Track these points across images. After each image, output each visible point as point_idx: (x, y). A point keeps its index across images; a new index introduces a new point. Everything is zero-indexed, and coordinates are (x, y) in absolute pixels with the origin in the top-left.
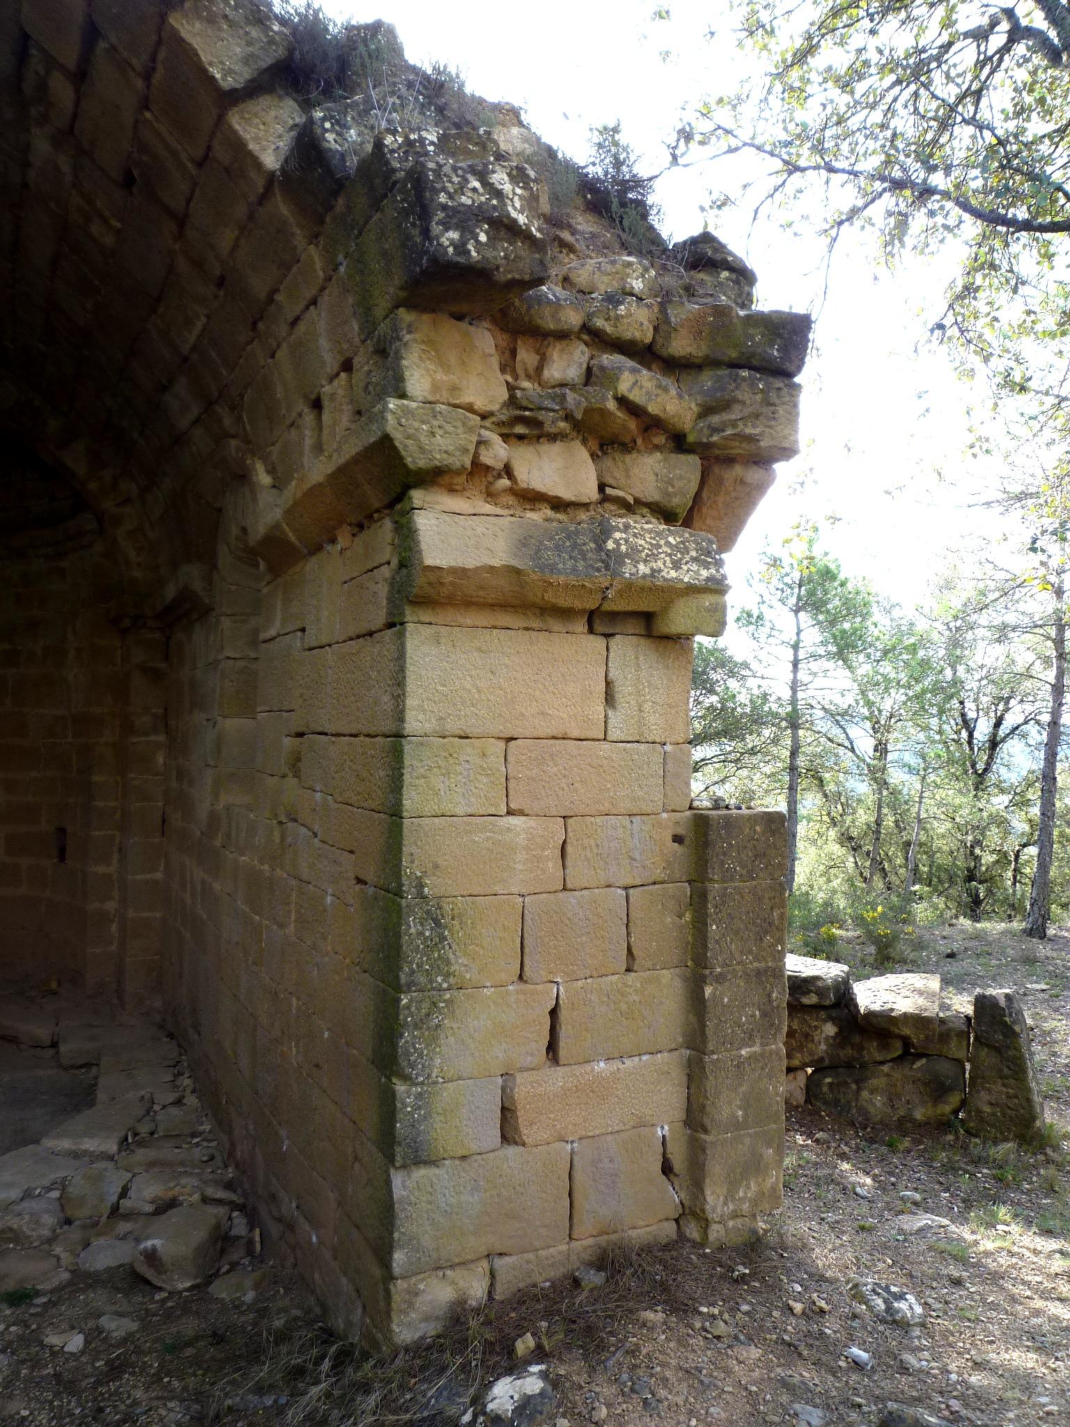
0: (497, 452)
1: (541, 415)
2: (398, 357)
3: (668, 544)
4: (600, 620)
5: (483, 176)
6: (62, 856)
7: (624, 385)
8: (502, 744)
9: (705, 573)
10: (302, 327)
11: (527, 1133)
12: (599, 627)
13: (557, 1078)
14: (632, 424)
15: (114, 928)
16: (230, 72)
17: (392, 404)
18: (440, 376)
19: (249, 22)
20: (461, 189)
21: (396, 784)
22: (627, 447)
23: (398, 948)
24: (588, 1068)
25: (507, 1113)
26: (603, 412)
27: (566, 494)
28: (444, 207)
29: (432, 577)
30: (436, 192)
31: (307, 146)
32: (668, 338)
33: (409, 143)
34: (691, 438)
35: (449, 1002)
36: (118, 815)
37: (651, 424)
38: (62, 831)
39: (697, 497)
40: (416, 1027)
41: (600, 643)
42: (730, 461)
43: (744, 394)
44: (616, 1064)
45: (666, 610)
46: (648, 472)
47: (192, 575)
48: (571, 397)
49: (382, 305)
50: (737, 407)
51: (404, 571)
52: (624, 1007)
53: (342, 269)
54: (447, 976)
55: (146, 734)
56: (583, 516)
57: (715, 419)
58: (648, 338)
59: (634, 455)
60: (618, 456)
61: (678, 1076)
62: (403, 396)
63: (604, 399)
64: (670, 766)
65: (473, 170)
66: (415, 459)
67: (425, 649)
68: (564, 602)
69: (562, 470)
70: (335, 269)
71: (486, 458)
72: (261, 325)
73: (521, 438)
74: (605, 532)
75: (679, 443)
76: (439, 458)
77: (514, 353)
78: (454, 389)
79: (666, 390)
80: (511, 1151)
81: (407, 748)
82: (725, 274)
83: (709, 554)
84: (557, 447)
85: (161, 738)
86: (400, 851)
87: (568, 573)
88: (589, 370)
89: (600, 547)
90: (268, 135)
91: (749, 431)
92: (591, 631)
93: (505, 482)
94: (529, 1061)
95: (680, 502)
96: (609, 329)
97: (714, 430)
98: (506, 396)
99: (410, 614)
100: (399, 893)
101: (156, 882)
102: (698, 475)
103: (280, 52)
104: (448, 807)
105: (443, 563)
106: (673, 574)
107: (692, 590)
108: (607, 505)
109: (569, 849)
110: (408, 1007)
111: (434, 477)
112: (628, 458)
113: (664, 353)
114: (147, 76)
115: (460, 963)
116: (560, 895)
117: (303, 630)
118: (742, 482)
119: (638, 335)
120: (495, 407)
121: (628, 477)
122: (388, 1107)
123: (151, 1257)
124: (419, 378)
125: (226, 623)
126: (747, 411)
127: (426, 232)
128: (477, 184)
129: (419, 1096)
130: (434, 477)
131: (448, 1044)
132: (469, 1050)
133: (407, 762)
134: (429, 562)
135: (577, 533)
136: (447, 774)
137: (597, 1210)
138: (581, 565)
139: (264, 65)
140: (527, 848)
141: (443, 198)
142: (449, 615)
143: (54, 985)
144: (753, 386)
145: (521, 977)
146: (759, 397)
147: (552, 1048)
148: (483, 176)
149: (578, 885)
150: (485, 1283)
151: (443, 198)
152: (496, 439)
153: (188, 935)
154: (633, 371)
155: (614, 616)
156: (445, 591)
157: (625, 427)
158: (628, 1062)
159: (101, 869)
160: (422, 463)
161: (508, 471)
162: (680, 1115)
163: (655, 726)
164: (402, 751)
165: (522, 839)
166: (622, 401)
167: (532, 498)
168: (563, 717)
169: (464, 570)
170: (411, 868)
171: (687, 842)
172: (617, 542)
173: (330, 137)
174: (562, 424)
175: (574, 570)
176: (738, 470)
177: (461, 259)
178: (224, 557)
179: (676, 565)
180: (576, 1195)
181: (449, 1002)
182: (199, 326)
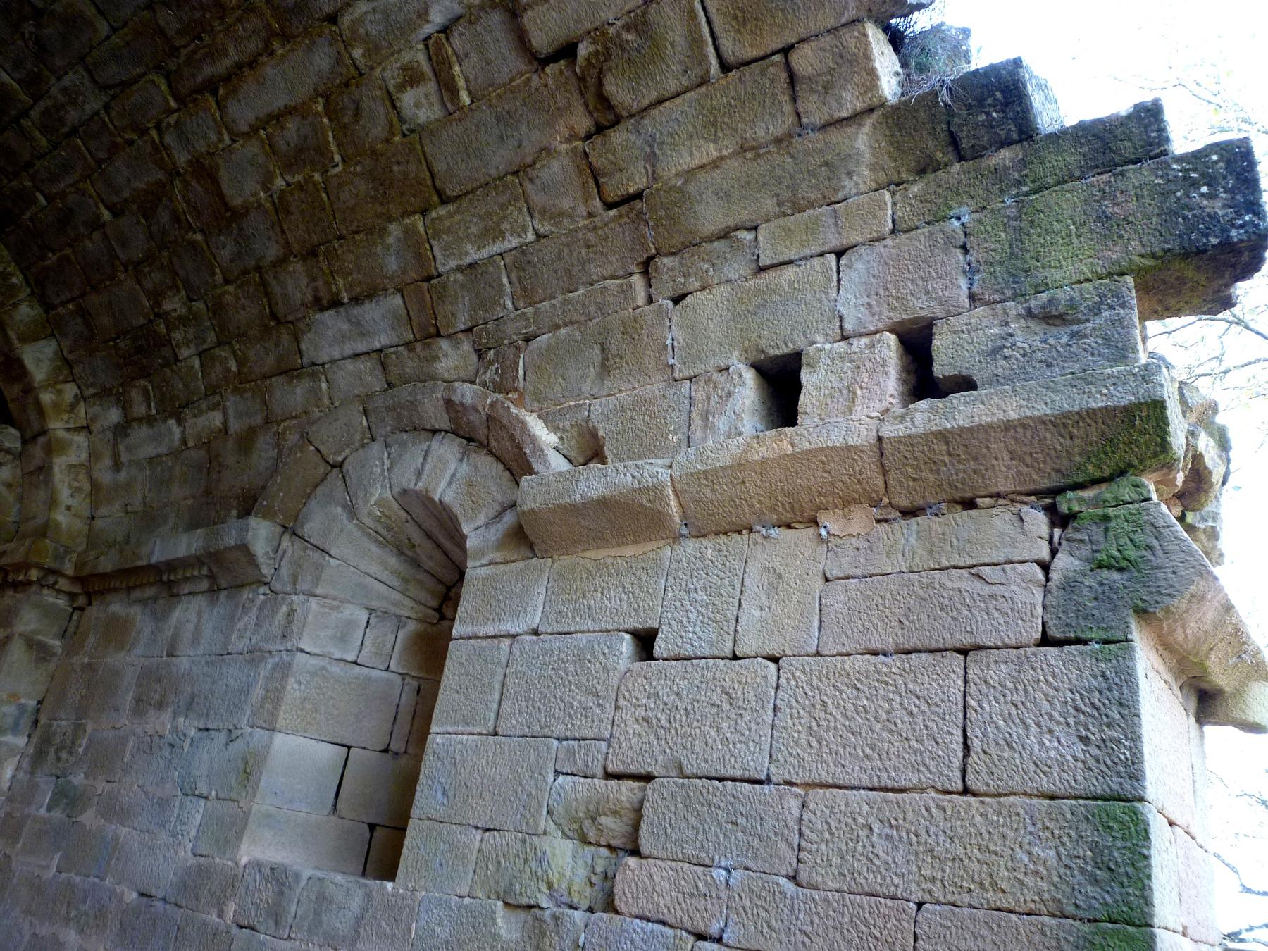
85: (21, 741)
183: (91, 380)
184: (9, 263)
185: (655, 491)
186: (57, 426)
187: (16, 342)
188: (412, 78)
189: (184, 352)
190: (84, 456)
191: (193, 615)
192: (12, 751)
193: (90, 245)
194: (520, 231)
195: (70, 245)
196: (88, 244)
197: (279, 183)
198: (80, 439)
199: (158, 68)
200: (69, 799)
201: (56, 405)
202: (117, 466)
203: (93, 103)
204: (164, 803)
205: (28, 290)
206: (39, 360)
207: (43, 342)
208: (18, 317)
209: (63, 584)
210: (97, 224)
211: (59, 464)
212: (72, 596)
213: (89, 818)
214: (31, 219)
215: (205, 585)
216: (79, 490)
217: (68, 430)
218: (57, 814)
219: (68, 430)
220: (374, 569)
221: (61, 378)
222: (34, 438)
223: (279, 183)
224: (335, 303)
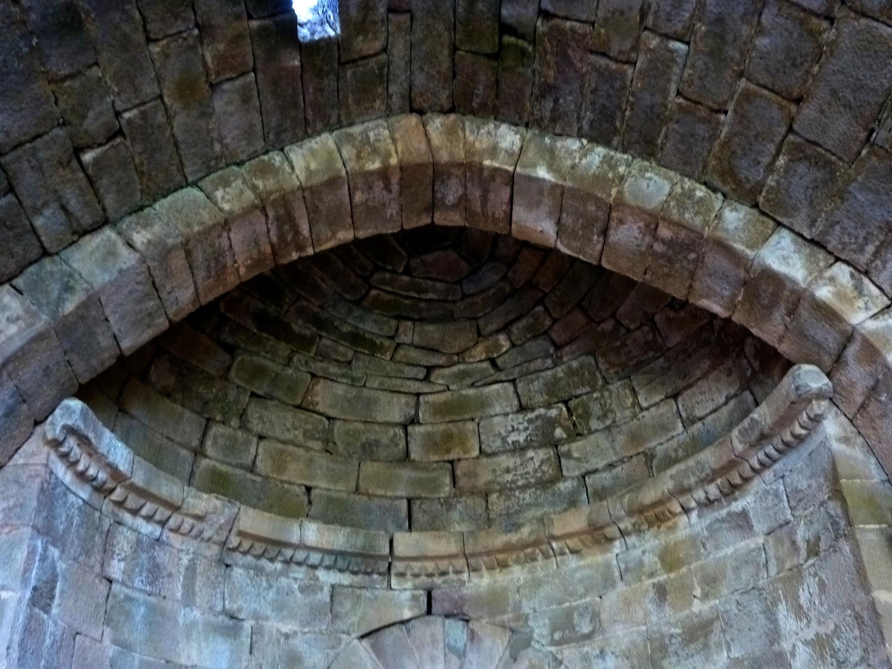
183: (862, 234)
184: (682, 181)
187: (749, 252)
195: (741, 75)
196: (763, 42)
201: (840, 295)
205: (720, 196)
206: (785, 258)
207: (774, 238)
208: (731, 227)
214: (679, 93)
217: (874, 316)
219: (874, 316)
221: (822, 264)
222: (839, 359)
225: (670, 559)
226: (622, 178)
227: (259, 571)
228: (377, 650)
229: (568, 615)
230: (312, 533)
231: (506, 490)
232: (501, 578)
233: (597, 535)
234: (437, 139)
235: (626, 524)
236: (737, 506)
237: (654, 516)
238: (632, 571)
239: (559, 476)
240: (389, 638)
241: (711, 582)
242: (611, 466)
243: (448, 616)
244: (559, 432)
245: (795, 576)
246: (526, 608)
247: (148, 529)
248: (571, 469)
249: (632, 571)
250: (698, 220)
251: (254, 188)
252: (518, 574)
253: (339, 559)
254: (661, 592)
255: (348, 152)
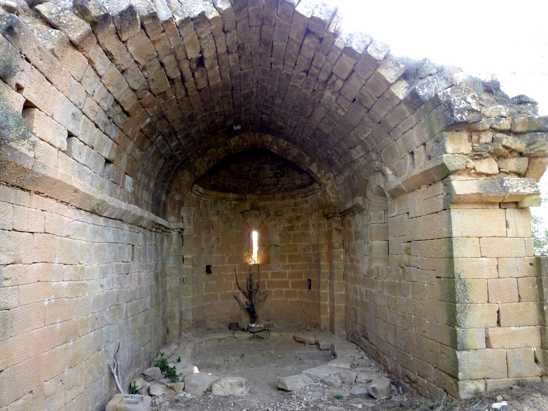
0: (472, 164)
1: (482, 153)
2: (444, 143)
3: (521, 183)
4: (503, 205)
5: (465, 100)
6: (310, 287)
7: (504, 142)
8: (478, 239)
9: (533, 190)
10: (407, 134)
11: (493, 345)
12: (502, 206)
13: (500, 330)
14: (507, 151)
15: (329, 310)
16: (392, 79)
17: (445, 155)
18: (455, 147)
19: (395, 66)
20: (460, 104)
21: (451, 249)
22: (505, 157)
23: (455, 292)
24: (509, 328)
25: (487, 339)
26: (499, 150)
27: (490, 172)
28: (457, 109)
29: (458, 197)
30: (454, 106)
31: (414, 95)
32: (515, 127)
33: (444, 93)
34: (524, 153)
35: (469, 307)
36: (328, 274)
37: (512, 151)
38: (310, 280)
39: (528, 169)
40: (461, 313)
41: (503, 211)
42: (537, 157)
43: (540, 139)
44: (517, 328)
45: (522, 201)
46: (512, 164)
47: (359, 200)
48: (490, 147)
49: (437, 131)
50: (538, 143)
51: (449, 196)
52: (519, 312)
53: (422, 121)
54: (468, 300)
55: (338, 249)
56: (495, 177)
57: (531, 147)
58: (509, 128)
59: (508, 159)
60: (503, 160)
61: (538, 333)
62: (446, 153)
63: (499, 146)
64: (527, 244)
65: (462, 99)
66: (451, 168)
67: (456, 215)
68: (493, 201)
69: (488, 166)
70: (421, 121)
71: (469, 166)
72: (391, 133)
73: (476, 159)
74: (502, 181)
75: (521, 154)
76: (457, 167)
77: (471, 137)
78: (458, 149)
79: (516, 142)
80: (489, 349)
81: (453, 240)
82: (529, 104)
83: (533, 184)
84: (486, 160)
85: (342, 250)
86: (453, 267)
87: (494, 194)
88: (493, 139)
89: (502, 186)
90: (401, 91)
91: (542, 149)
92: (500, 208)
93: (473, 171)
94: (492, 325)
95: (522, 171)
96: (498, 128)
97: (531, 150)
98: (472, 149)
99: (451, 207)
100: (454, 278)
101: (342, 294)
102: (528, 162)
103: (403, 72)
104: (465, 255)
105: (461, 193)
106: (523, 191)
107: (530, 195)
108: (501, 174)
109: (499, 267)
110: (458, 307)
111: (456, 172)
112: (506, 160)
113: (514, 131)
114: (366, 80)
115: (471, 296)
116: (498, 279)
117: (408, 213)
118: (541, 163)
119: (506, 128)
120: (469, 152)
121: (506, 165)
122: (454, 334)
123: (374, 389)
124: (450, 148)
125: (371, 213)
126: (541, 144)
127: (452, 116)
128: (464, 102)
129: (463, 331)
130: (456, 172)
131: (470, 318)
132: (475, 322)
133: (454, 244)
134: (457, 193)
135: (495, 182)
136: (464, 247)
137: (515, 370)
138: (497, 191)
139: (400, 76)
140: (487, 266)
141: (456, 107)
142: (462, 206)
143: (309, 328)
144: (542, 136)
145: (488, 302)
146: (544, 139)
147: (498, 322)
148: (465, 100)
149: (502, 277)
150: (484, 386)
151: (456, 107)
152: (471, 160)
153: (359, 309)
154: (507, 138)
155: (506, 203)
156: (461, 200)
157: (505, 153)
158: (522, 328)
159: (324, 291)
160: (453, 169)
161: (474, 169)
162: (539, 345)
163: (521, 233)
164: (452, 241)
165: (486, 264)
166: (505, 147)
167: (480, 174)
168: (494, 231)
169: (466, 195)
170: (457, 270)
171: (534, 265)
172: (506, 184)
173: (420, 92)
174: (488, 154)
175: (496, 192)
176: (540, 159)
177: (462, 121)
178: (369, 193)
179: (524, 188)
180: (509, 364)
181: (469, 307)
182: (369, 133)
185: (400, 185)
186: (323, 181)
188: (337, 109)
189: (336, 161)
190: (331, 185)
191: (358, 217)
192: (342, 252)
193: (310, 144)
194: (369, 131)
197: (330, 129)
198: (329, 181)
199: (301, 115)
200: (352, 260)
202: (337, 186)
203: (295, 123)
204: (362, 258)
209: (338, 215)
210: (309, 141)
211: (327, 189)
212: (341, 217)
213: (355, 263)
215: (357, 211)
216: (333, 193)
218: (351, 263)
220: (382, 201)
223: (330, 129)
224: (352, 148)
225: (295, 204)
226: (289, 149)
227: (222, 202)
228: (243, 215)
229: (277, 211)
230: (231, 195)
231: (268, 185)
232: (266, 203)
233: (283, 198)
234: (257, 138)
235: (289, 197)
236: (307, 199)
237: (294, 197)
238: (289, 205)
239: (278, 184)
240: (245, 213)
241: (301, 210)
242: (288, 184)
243: (256, 209)
244: (279, 175)
245: (312, 214)
246: (270, 209)
247: (204, 199)
248: (280, 183)
249: (289, 205)
250: (301, 159)
251: (224, 149)
252: (269, 203)
253: (236, 200)
254: (293, 210)
255: (241, 141)
